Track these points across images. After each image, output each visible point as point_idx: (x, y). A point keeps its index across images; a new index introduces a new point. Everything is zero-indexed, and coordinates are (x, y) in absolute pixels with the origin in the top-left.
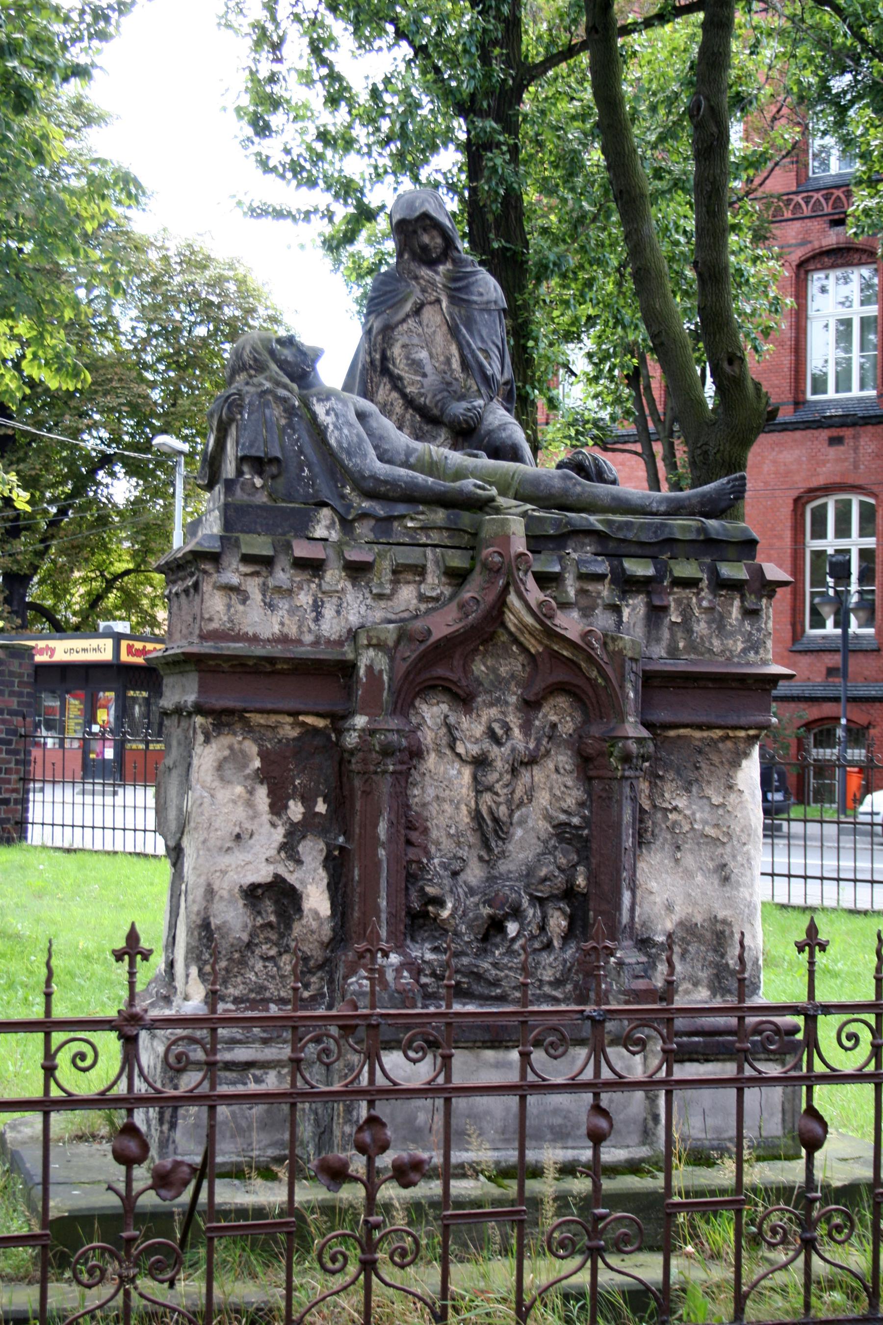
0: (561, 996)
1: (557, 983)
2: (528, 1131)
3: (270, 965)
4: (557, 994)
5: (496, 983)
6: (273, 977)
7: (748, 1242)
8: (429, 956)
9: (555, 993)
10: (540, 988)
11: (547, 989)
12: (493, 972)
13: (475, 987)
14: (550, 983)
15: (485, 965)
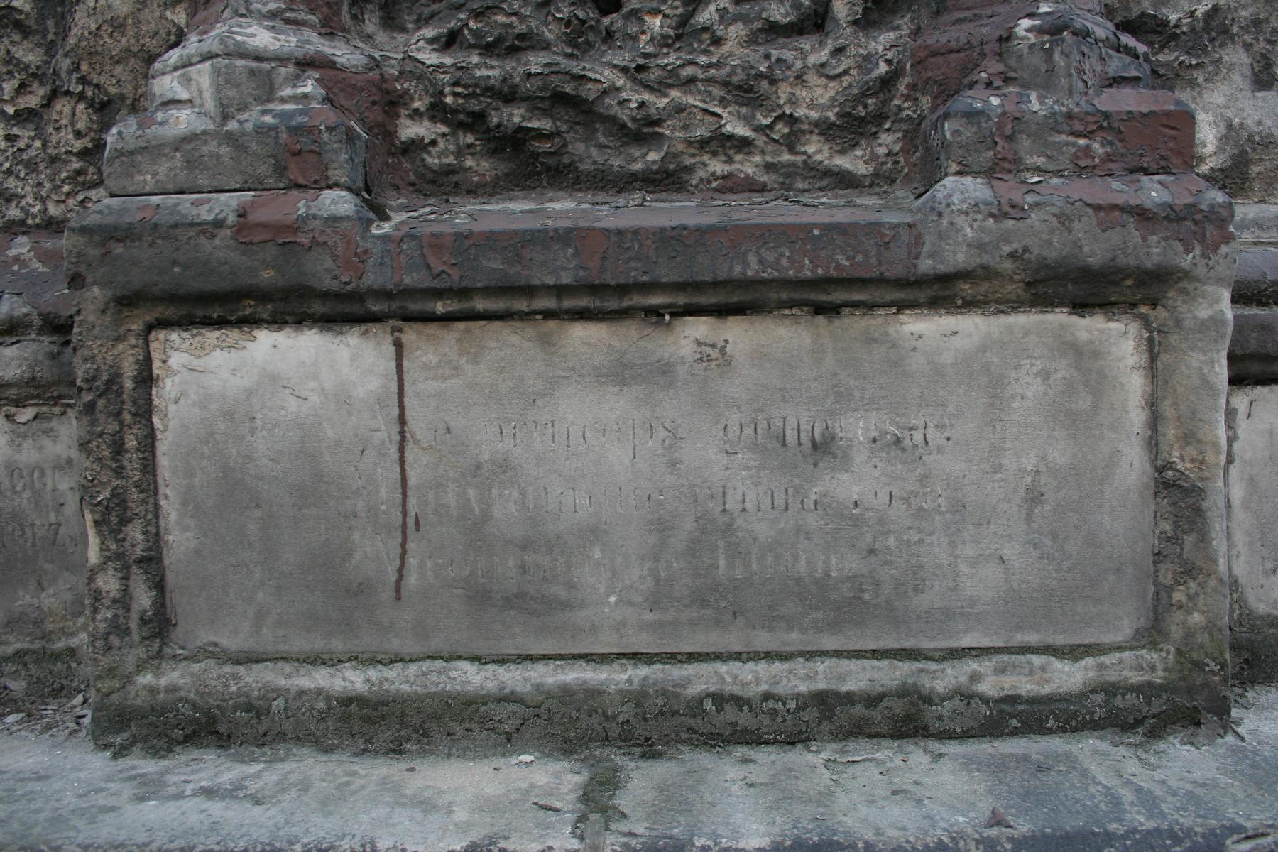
0: (862, 169)
1: (850, 127)
2: (399, 534)
3: (24, 133)
4: (854, 162)
5: (643, 131)
6: (31, 166)
7: (182, 75)
8: (430, 57)
9: (843, 162)
10: (791, 143)
11: (816, 149)
12: (634, 96)
13: (578, 148)
14: (825, 129)
15: (604, 70)
